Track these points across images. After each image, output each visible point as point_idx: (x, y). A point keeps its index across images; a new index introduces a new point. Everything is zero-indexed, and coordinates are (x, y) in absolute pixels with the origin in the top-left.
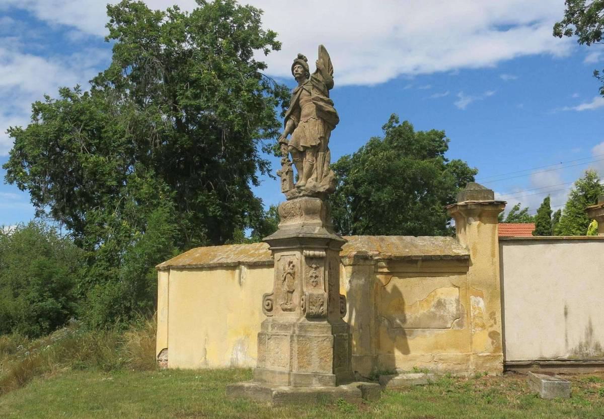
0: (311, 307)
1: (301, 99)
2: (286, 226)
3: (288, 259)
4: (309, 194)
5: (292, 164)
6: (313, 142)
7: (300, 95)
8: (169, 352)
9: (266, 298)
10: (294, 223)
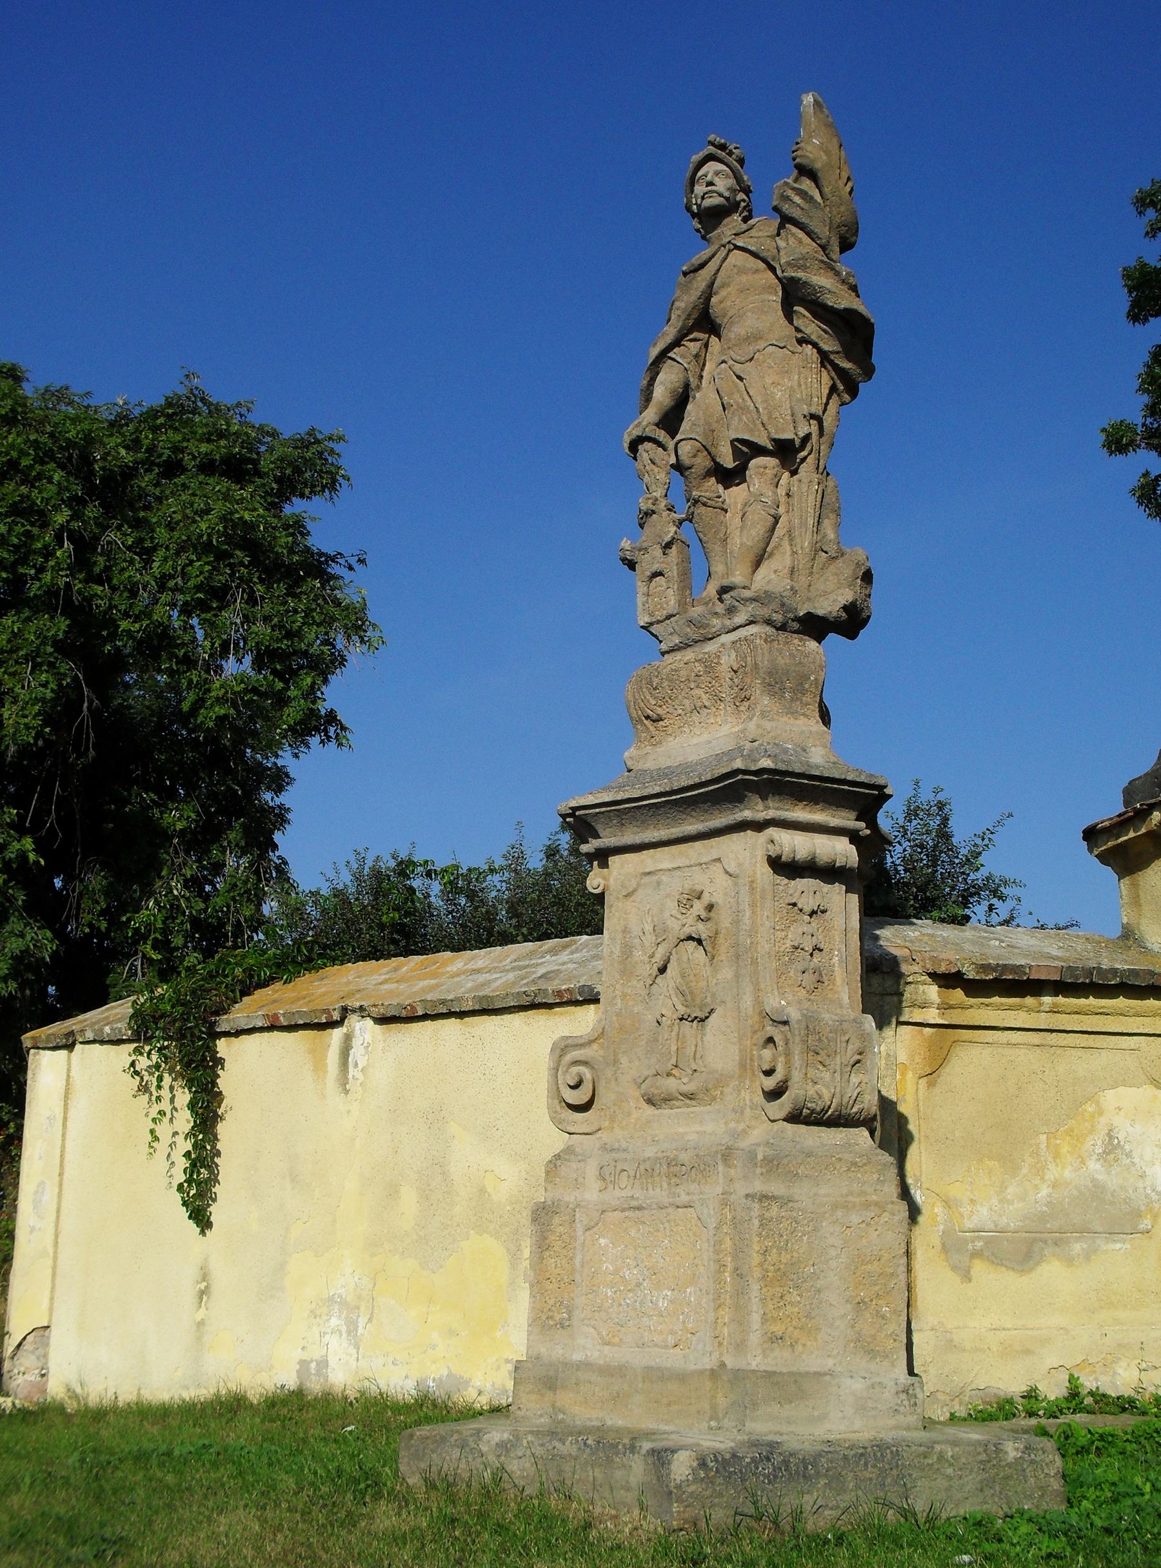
0: (812, 1073)
1: (724, 285)
3: (676, 885)
8: (53, 1341)
9: (568, 1058)
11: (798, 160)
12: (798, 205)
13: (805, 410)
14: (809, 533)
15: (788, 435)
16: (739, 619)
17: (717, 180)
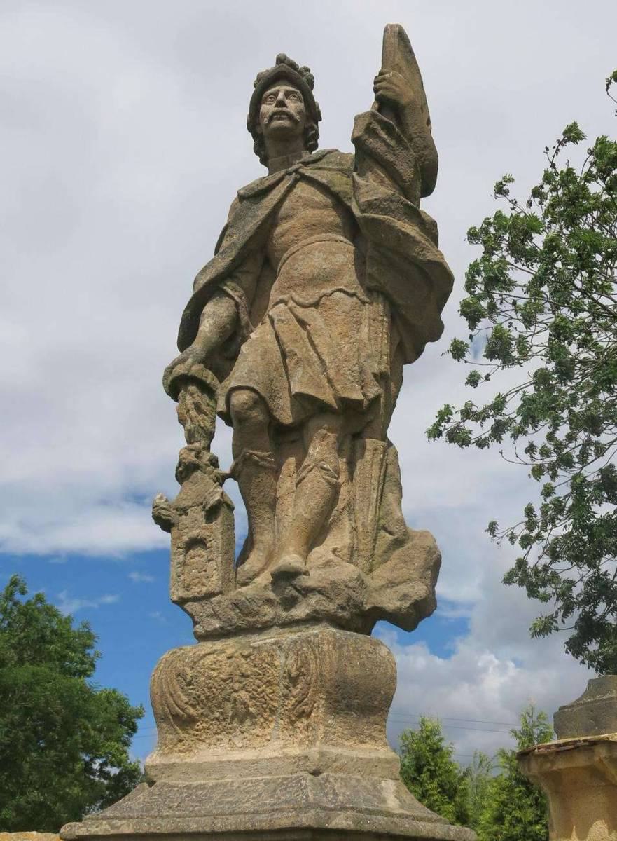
1: (288, 217)
2: (201, 769)
4: (341, 614)
5: (225, 477)
6: (353, 389)
7: (282, 200)
10: (249, 755)
11: (381, 92)
12: (384, 141)
13: (376, 368)
14: (372, 509)
15: (357, 395)
16: (300, 611)
17: (287, 102)
